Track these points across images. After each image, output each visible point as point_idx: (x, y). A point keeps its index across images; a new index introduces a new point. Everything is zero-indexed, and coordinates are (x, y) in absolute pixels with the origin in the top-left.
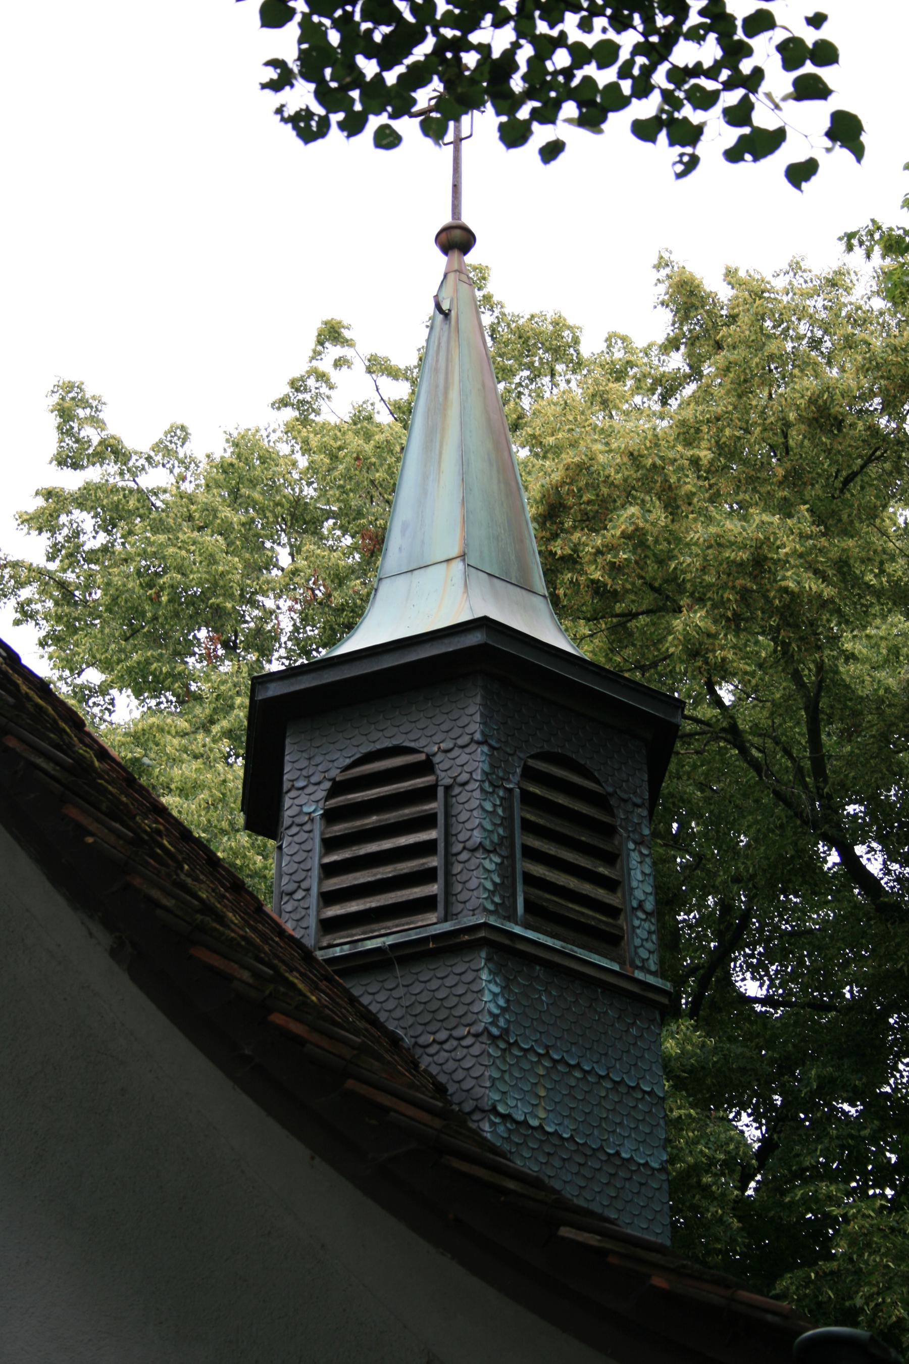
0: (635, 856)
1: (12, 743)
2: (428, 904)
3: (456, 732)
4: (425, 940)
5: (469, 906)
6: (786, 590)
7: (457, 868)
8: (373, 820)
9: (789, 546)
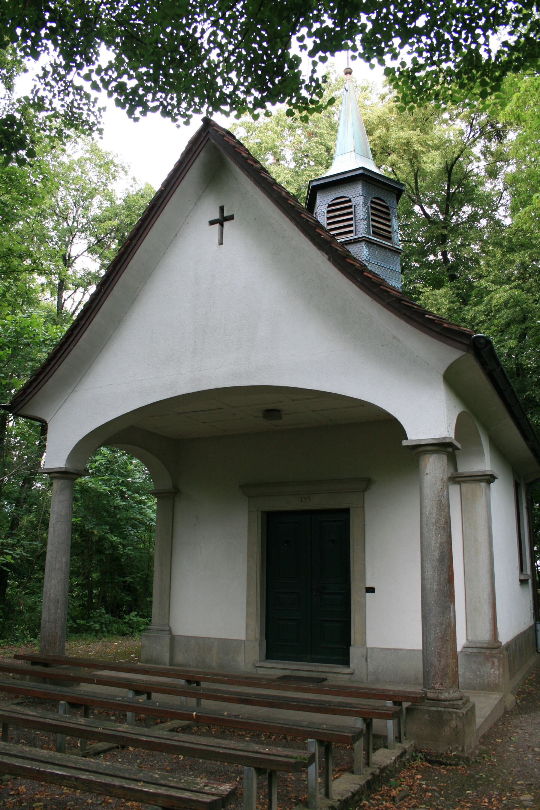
0: (394, 220)
1: (303, 216)
2: (351, 232)
3: (356, 193)
4: (351, 240)
5: (361, 232)
6: (414, 150)
7: (357, 224)
8: (338, 213)
9: (415, 139)
